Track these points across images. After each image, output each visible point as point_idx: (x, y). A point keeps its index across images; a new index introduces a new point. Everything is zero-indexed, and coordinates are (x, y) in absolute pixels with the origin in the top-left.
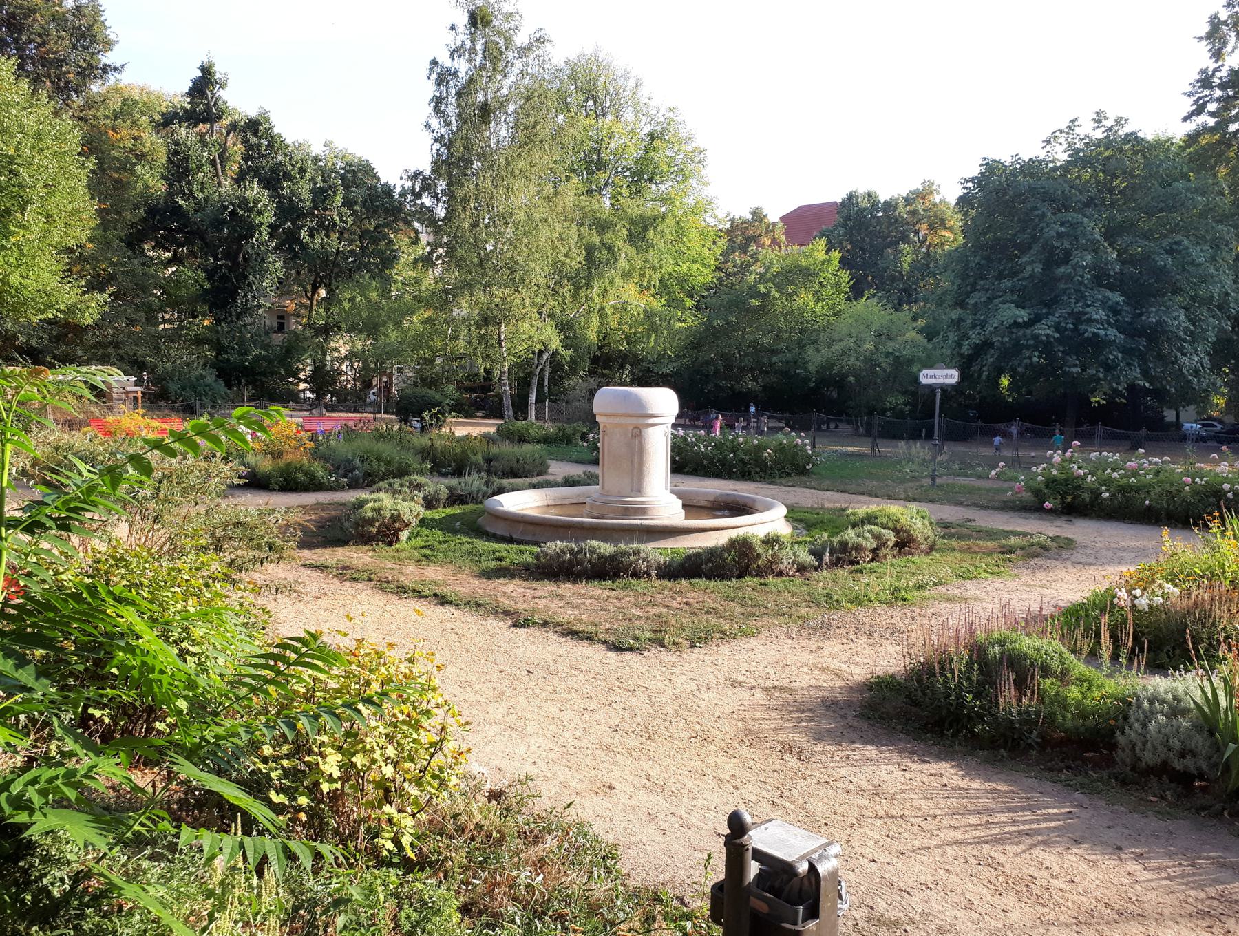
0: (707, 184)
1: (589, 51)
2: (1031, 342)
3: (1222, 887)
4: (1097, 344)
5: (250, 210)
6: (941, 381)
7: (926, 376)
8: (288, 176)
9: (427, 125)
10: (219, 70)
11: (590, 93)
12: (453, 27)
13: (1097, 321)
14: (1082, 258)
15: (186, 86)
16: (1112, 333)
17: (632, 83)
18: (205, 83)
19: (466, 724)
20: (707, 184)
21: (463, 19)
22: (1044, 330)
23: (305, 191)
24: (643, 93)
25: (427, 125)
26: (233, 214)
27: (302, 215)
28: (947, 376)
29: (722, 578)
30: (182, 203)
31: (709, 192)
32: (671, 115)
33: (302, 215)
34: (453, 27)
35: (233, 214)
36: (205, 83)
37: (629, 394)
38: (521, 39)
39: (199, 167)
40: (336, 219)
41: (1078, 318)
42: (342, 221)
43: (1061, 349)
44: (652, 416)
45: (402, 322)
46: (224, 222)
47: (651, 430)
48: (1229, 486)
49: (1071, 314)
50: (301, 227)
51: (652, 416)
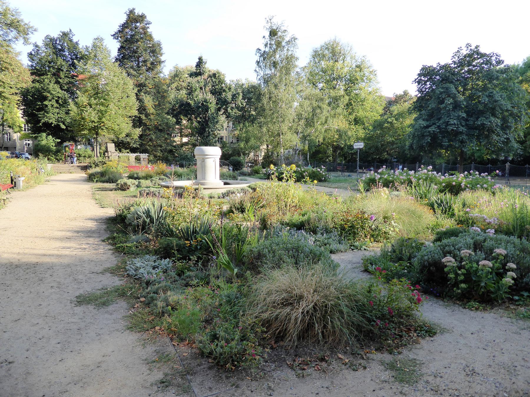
0: (378, 83)
1: (333, 38)
2: (428, 134)
3: (400, 334)
4: (457, 133)
5: (208, 103)
6: (358, 147)
7: (362, 145)
8: (224, 91)
9: (255, 71)
10: (204, 59)
11: (334, 53)
12: (264, 37)
14: (448, 100)
15: (194, 64)
17: (349, 49)
18: (200, 63)
19: (493, 371)
20: (378, 83)
21: (267, 34)
22: (432, 129)
23: (229, 96)
24: (353, 52)
25: (255, 71)
26: (202, 104)
27: (228, 103)
28: (360, 145)
29: (110, 183)
30: (190, 102)
31: (378, 86)
32: (363, 58)
33: (228, 103)
34: (264, 37)
35: (202, 104)
36: (200, 63)
37: (200, 148)
38: (287, 39)
39: (196, 90)
40: (240, 104)
41: (447, 124)
42: (242, 104)
43: (441, 136)
44: (207, 155)
45: (502, 160)
46: (200, 107)
47: (207, 160)
48: (486, 186)
49: (444, 123)
50: (228, 107)
51: (207, 155)
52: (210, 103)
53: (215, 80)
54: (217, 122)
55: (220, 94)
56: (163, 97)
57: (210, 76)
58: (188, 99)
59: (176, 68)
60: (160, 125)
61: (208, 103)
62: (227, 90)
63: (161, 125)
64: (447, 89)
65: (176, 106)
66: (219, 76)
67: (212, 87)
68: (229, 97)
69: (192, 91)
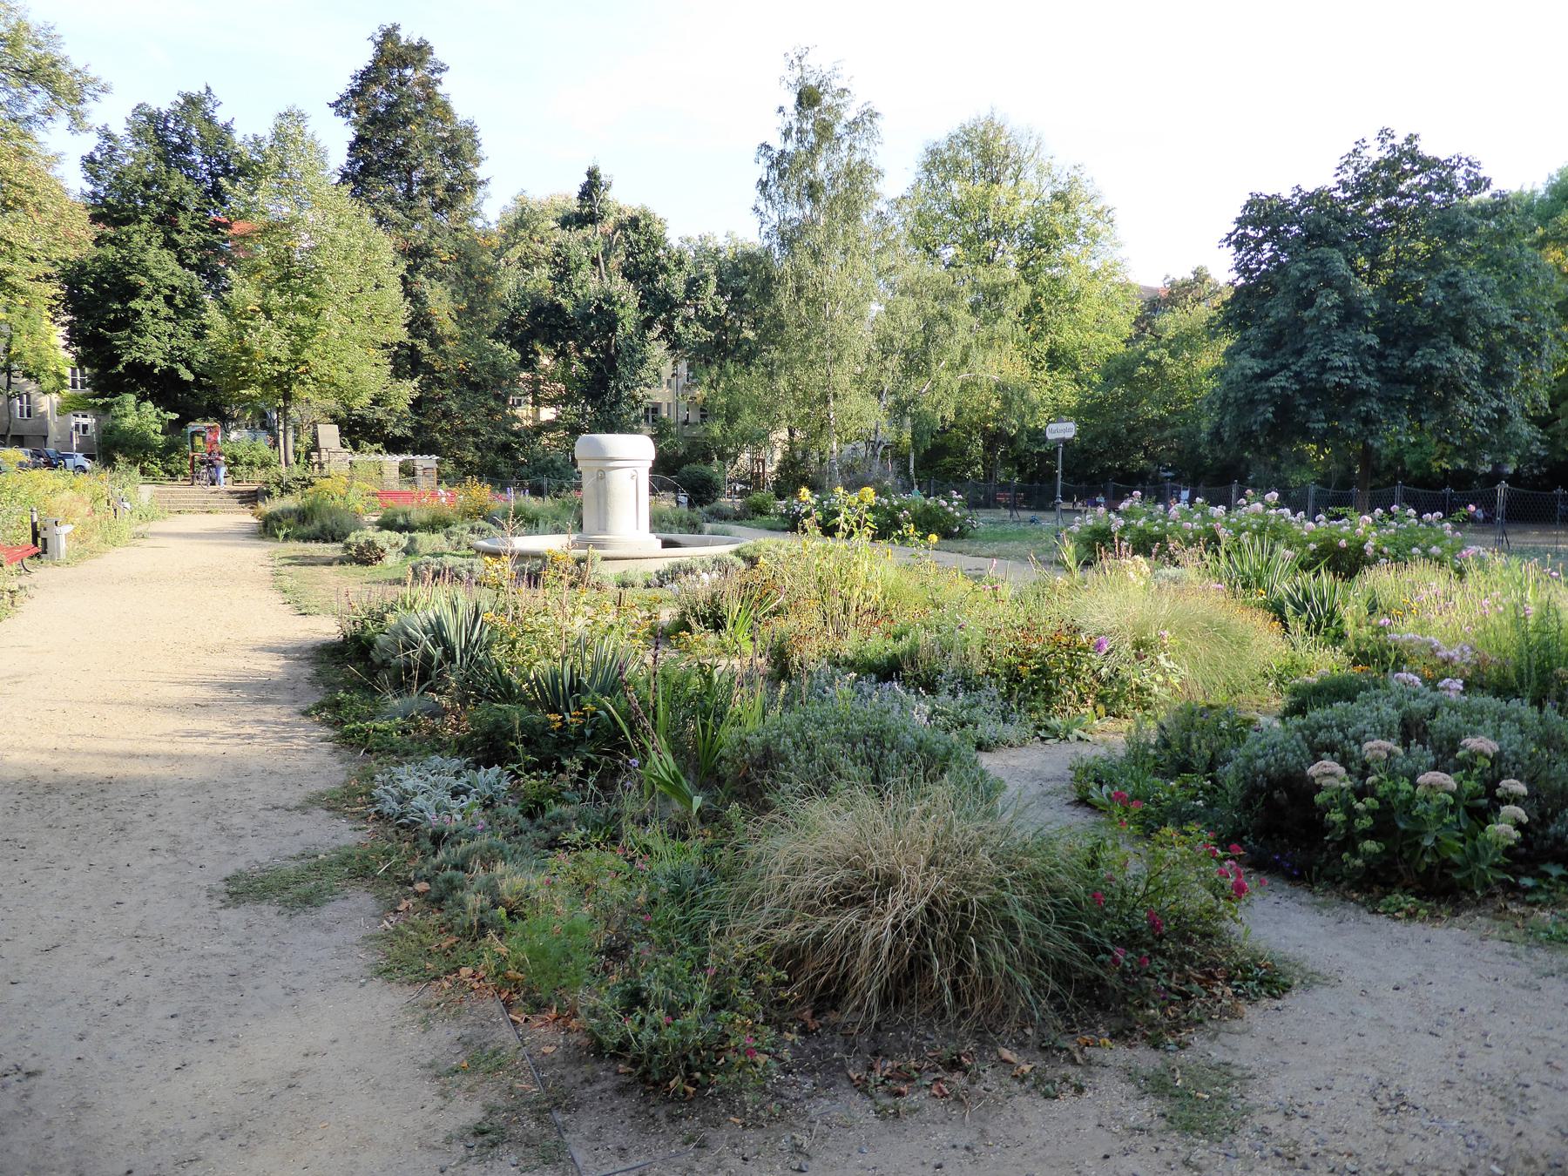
0: (1119, 245)
1: (984, 113)
2: (1266, 396)
5: (614, 304)
6: (1061, 436)
7: (1070, 430)
9: (756, 209)
10: (604, 173)
11: (987, 157)
12: (781, 109)
13: (1339, 368)
14: (1327, 298)
15: (575, 191)
16: (1365, 381)
17: (1033, 144)
18: (592, 186)
20: (1119, 245)
21: (791, 100)
22: (1278, 382)
23: (678, 286)
24: (1044, 153)
25: (756, 209)
26: (599, 308)
27: (675, 305)
28: (1065, 431)
29: (326, 541)
30: (563, 301)
31: (1120, 254)
32: (1075, 173)
33: (675, 305)
34: (781, 109)
35: (599, 308)
36: (592, 186)
37: (593, 439)
38: (850, 115)
41: (1323, 366)
42: (716, 309)
43: (1303, 402)
44: (612, 460)
46: (591, 316)
47: (613, 473)
48: (1439, 551)
49: (1314, 363)
50: (674, 318)
51: (612, 460)
52: (623, 306)
53: (636, 237)
54: (642, 362)
55: (651, 277)
57: (621, 226)
58: (555, 294)
59: (521, 200)
60: (474, 370)
61: (614, 304)
62: (671, 266)
63: (476, 371)
65: (520, 315)
66: (647, 226)
67: (627, 258)
68: (677, 287)
69: (567, 269)
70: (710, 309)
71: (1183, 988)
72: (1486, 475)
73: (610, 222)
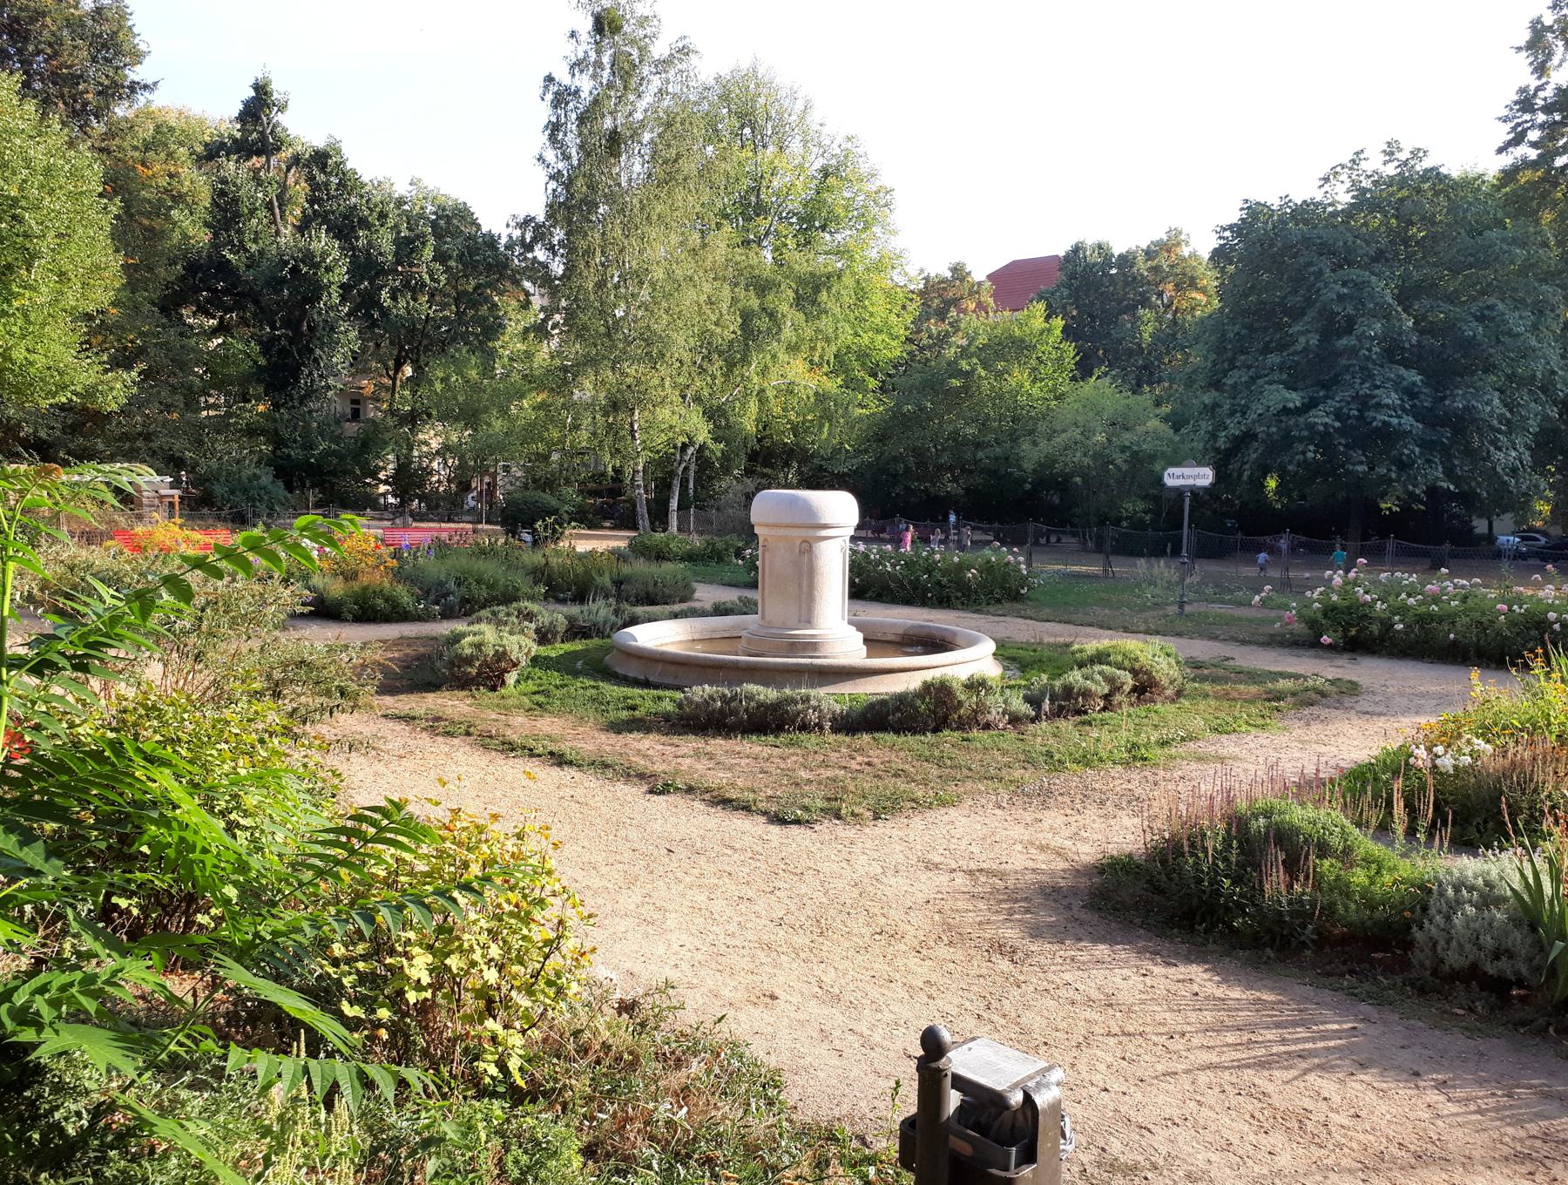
0: (894, 233)
1: (745, 65)
2: (1305, 433)
4: (1389, 436)
5: (316, 266)
6: (1190, 482)
7: (1172, 476)
8: (364, 223)
9: (541, 159)
10: (278, 89)
11: (746, 117)
12: (573, 35)
14: (1369, 326)
15: (236, 109)
16: (1408, 421)
17: (800, 106)
18: (259, 104)
20: (894, 233)
21: (585, 24)
22: (1321, 418)
23: (385, 242)
24: (814, 118)
25: (541, 159)
26: (295, 270)
27: (382, 272)
28: (1198, 476)
29: (914, 732)
30: (230, 256)
31: (897, 243)
32: (849, 145)
33: (382, 272)
34: (573, 35)
35: (295, 270)
36: (259, 104)
37: (796, 499)
38: (659, 50)
41: (1364, 403)
42: (433, 280)
43: (1343, 442)
44: (826, 527)
46: (283, 281)
47: (824, 545)
48: (1555, 615)
49: (1356, 398)
50: (381, 287)
51: (826, 527)
56: (153, 235)
64: (1359, 286)
70: (426, 277)
71: (1546, 1123)
72: (508, 408)
73: (286, 154)
